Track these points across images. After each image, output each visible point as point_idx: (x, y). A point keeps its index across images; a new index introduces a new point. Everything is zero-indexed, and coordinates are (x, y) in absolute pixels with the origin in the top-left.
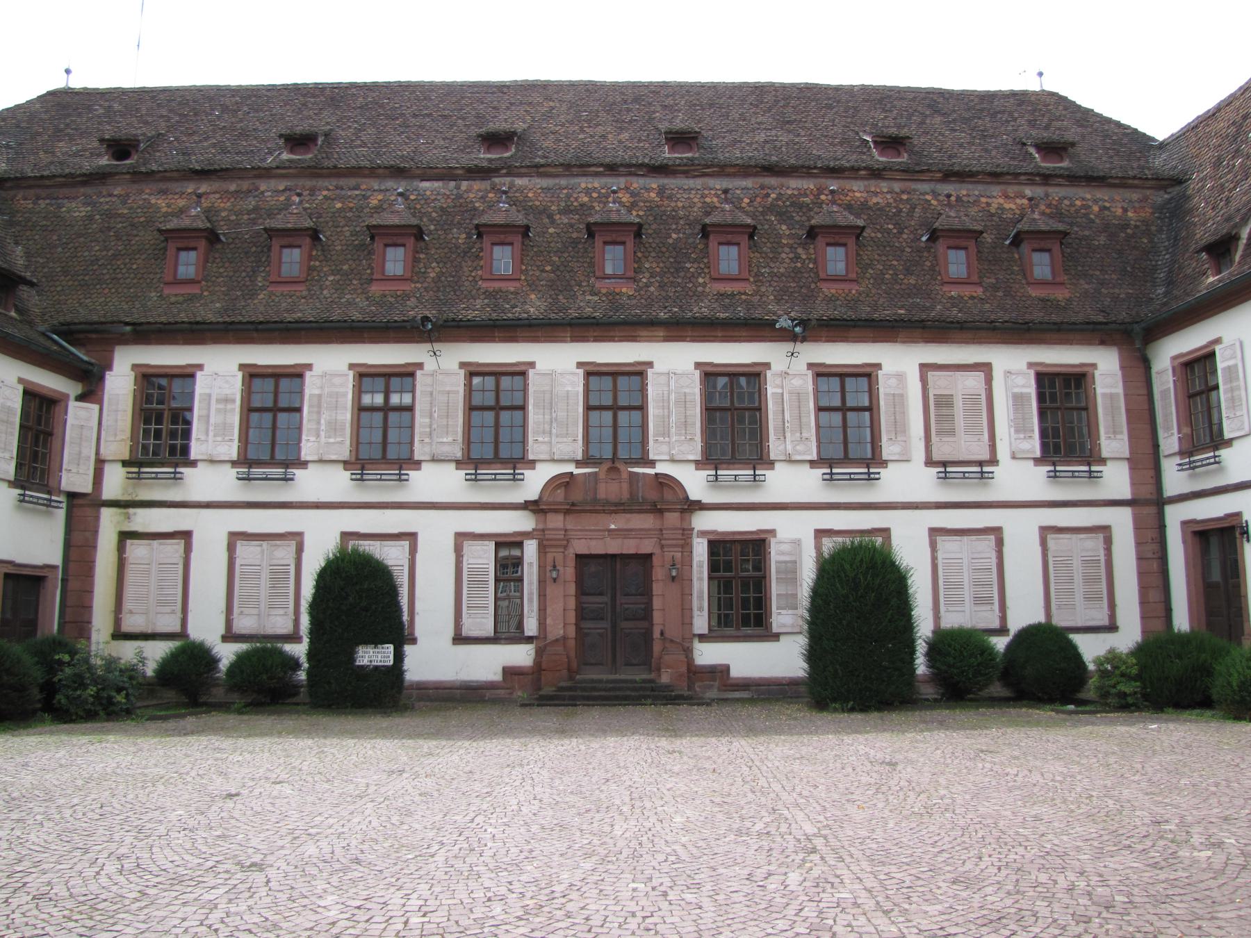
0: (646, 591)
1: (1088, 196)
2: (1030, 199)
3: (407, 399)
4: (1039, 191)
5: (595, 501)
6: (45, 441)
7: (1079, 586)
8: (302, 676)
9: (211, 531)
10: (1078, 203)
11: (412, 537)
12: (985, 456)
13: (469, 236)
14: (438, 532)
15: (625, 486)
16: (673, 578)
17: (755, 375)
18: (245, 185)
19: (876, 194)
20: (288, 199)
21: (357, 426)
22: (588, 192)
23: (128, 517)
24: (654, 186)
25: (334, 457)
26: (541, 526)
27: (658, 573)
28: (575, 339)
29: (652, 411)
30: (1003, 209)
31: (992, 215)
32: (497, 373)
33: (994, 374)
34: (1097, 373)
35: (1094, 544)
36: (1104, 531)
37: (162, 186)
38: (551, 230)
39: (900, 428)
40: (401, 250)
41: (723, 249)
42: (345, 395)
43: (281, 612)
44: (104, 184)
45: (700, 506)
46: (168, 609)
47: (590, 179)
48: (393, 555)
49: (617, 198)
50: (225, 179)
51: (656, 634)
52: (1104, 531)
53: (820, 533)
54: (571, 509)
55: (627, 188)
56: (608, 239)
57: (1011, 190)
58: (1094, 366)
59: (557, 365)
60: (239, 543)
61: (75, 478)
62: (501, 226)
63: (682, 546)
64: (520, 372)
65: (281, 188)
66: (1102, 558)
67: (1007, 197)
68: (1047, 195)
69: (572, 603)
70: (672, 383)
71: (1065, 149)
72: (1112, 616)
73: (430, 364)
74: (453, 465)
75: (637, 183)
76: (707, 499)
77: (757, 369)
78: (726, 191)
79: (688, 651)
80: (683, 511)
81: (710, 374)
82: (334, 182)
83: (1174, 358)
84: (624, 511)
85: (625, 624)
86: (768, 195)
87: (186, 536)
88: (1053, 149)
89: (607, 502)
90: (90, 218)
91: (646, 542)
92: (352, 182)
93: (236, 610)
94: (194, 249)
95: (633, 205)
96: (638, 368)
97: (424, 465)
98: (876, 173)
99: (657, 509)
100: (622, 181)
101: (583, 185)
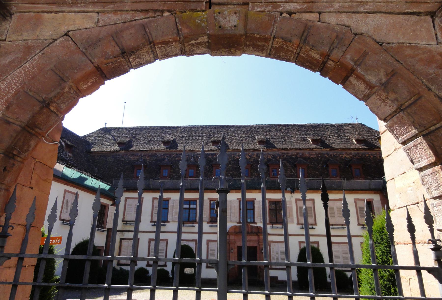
3: (195, 206)
13: (210, 167)
23: (123, 235)
30: (346, 158)
34: (374, 201)
58: (373, 199)
67: (347, 154)
90: (114, 161)
95: (250, 159)
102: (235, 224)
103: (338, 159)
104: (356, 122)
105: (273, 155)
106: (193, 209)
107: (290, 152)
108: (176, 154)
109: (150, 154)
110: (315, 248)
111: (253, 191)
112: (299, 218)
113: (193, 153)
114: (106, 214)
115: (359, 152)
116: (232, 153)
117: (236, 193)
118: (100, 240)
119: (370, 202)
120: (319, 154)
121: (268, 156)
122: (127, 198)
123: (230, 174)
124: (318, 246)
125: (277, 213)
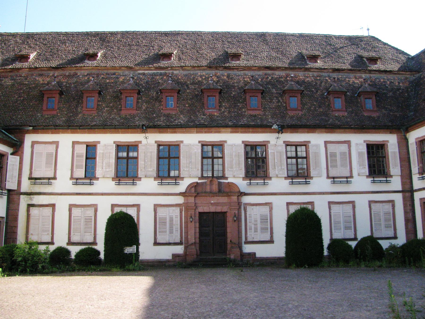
17: (264, 145)
23: (31, 199)
34: (389, 144)
67: (356, 78)
81: (247, 145)
90: (13, 85)
95: (218, 81)
102: (196, 180)
103: (343, 84)
104: (366, 34)
105: (252, 77)
107: (278, 73)
108: (107, 74)
109: (67, 74)
110: (309, 210)
111: (222, 130)
113: (132, 72)
115: (372, 75)
116: (192, 72)
117: (197, 132)
119: (384, 145)
120: (317, 76)
121: (244, 78)
122: (34, 143)
123: (188, 104)
125: (256, 164)
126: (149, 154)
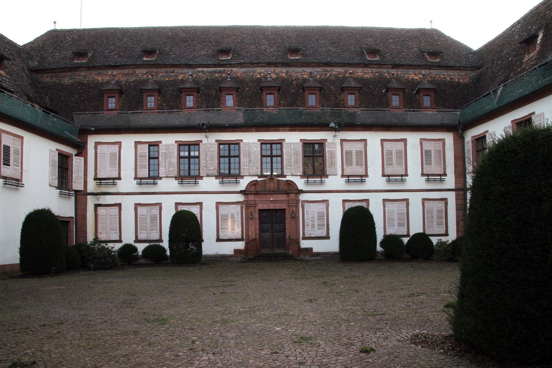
0: (283, 222)
1: (446, 74)
2: (424, 75)
3: (197, 154)
4: (427, 71)
5: (265, 190)
6: (66, 171)
7: (435, 220)
8: (168, 253)
9: (128, 203)
10: (442, 76)
11: (200, 204)
12: (364, 173)
13: (217, 91)
14: (210, 202)
15: (276, 185)
16: (293, 217)
17: (321, 144)
18: (131, 71)
19: (366, 73)
20: (148, 77)
21: (179, 164)
22: (260, 73)
23: (98, 200)
24: (284, 71)
25: (171, 175)
26: (246, 199)
27: (288, 216)
28: (257, 131)
29: (285, 157)
31: (410, 81)
32: (229, 144)
33: (408, 143)
35: (441, 205)
36: (445, 200)
37: (99, 71)
38: (247, 89)
39: (333, 164)
40: (192, 97)
41: (310, 96)
42: (174, 152)
43: (155, 231)
44: (77, 71)
45: (302, 192)
46: (114, 232)
47: (260, 68)
48: (195, 210)
49: (272, 73)
50: (123, 69)
51: (287, 237)
52: (445, 200)
53: (344, 201)
54: (257, 194)
55: (274, 72)
56: (268, 92)
57: (417, 71)
59: (251, 140)
60: (138, 207)
61: (78, 185)
62: (229, 88)
63: (296, 206)
64: (237, 143)
65: (145, 72)
66: (444, 210)
67: (415, 74)
68: (430, 73)
69: (258, 227)
70: (292, 147)
71: (438, 54)
72: (447, 230)
73: (205, 141)
74: (214, 178)
75: (278, 70)
76: (304, 189)
77: (322, 142)
78: (311, 73)
79: (298, 243)
80: (296, 193)
82: (165, 70)
83: (472, 137)
84: (276, 194)
85: (276, 234)
86: (326, 74)
87: (119, 205)
88: (434, 54)
89: (270, 191)
91: (283, 204)
92: (172, 70)
93: (139, 232)
94: (114, 97)
96: (280, 142)
97: (204, 178)
98: (366, 65)
99: (287, 193)
100: (272, 69)
101: (258, 71)
106: (195, 157)
112: (345, 167)
114: (70, 168)
118: (63, 208)
121: (303, 75)
124: (368, 205)
125: (315, 161)
126: (209, 153)
